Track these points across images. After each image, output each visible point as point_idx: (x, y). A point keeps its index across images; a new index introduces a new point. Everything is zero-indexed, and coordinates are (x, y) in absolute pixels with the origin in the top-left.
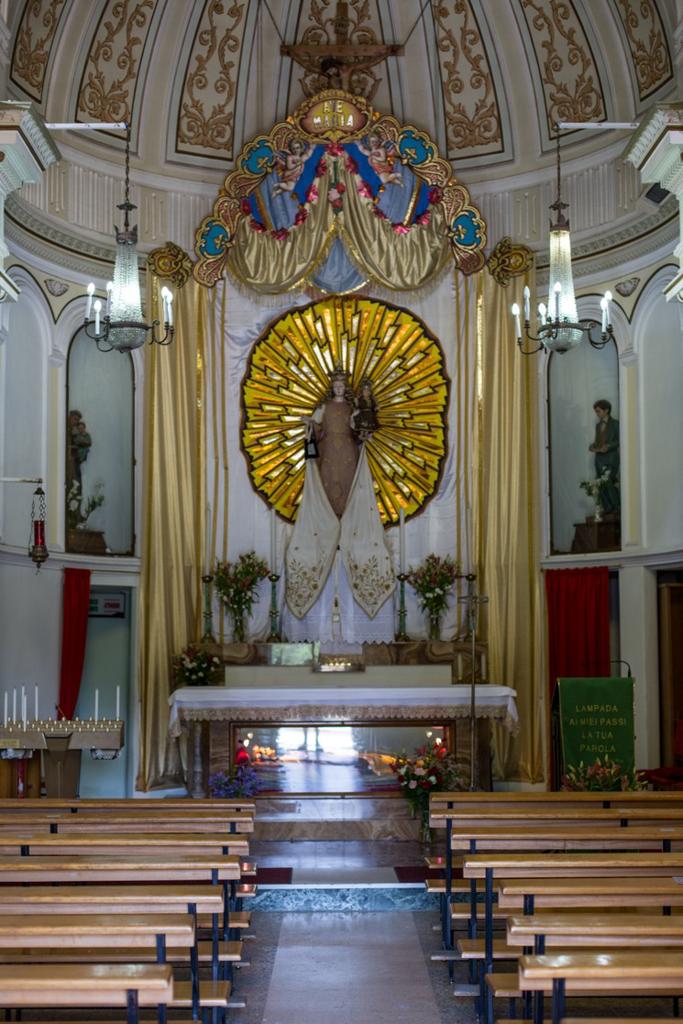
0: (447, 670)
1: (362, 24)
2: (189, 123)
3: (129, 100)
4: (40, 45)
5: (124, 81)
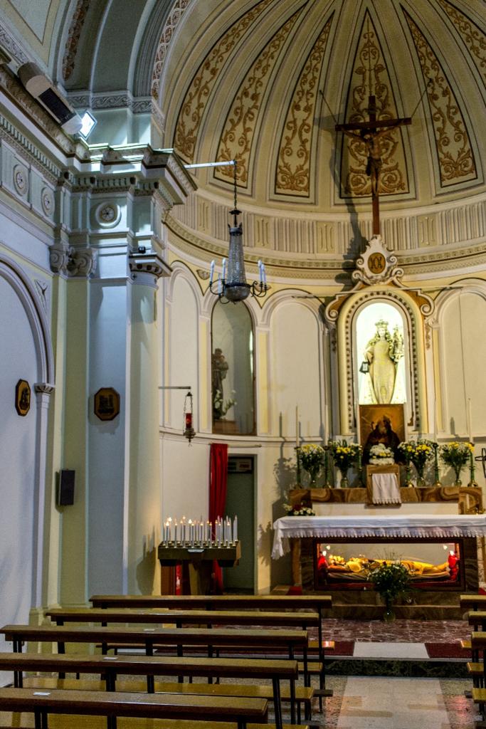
0: (456, 506)
1: (385, 110)
2: (282, 177)
3: (246, 165)
4: (191, 132)
5: (243, 154)
